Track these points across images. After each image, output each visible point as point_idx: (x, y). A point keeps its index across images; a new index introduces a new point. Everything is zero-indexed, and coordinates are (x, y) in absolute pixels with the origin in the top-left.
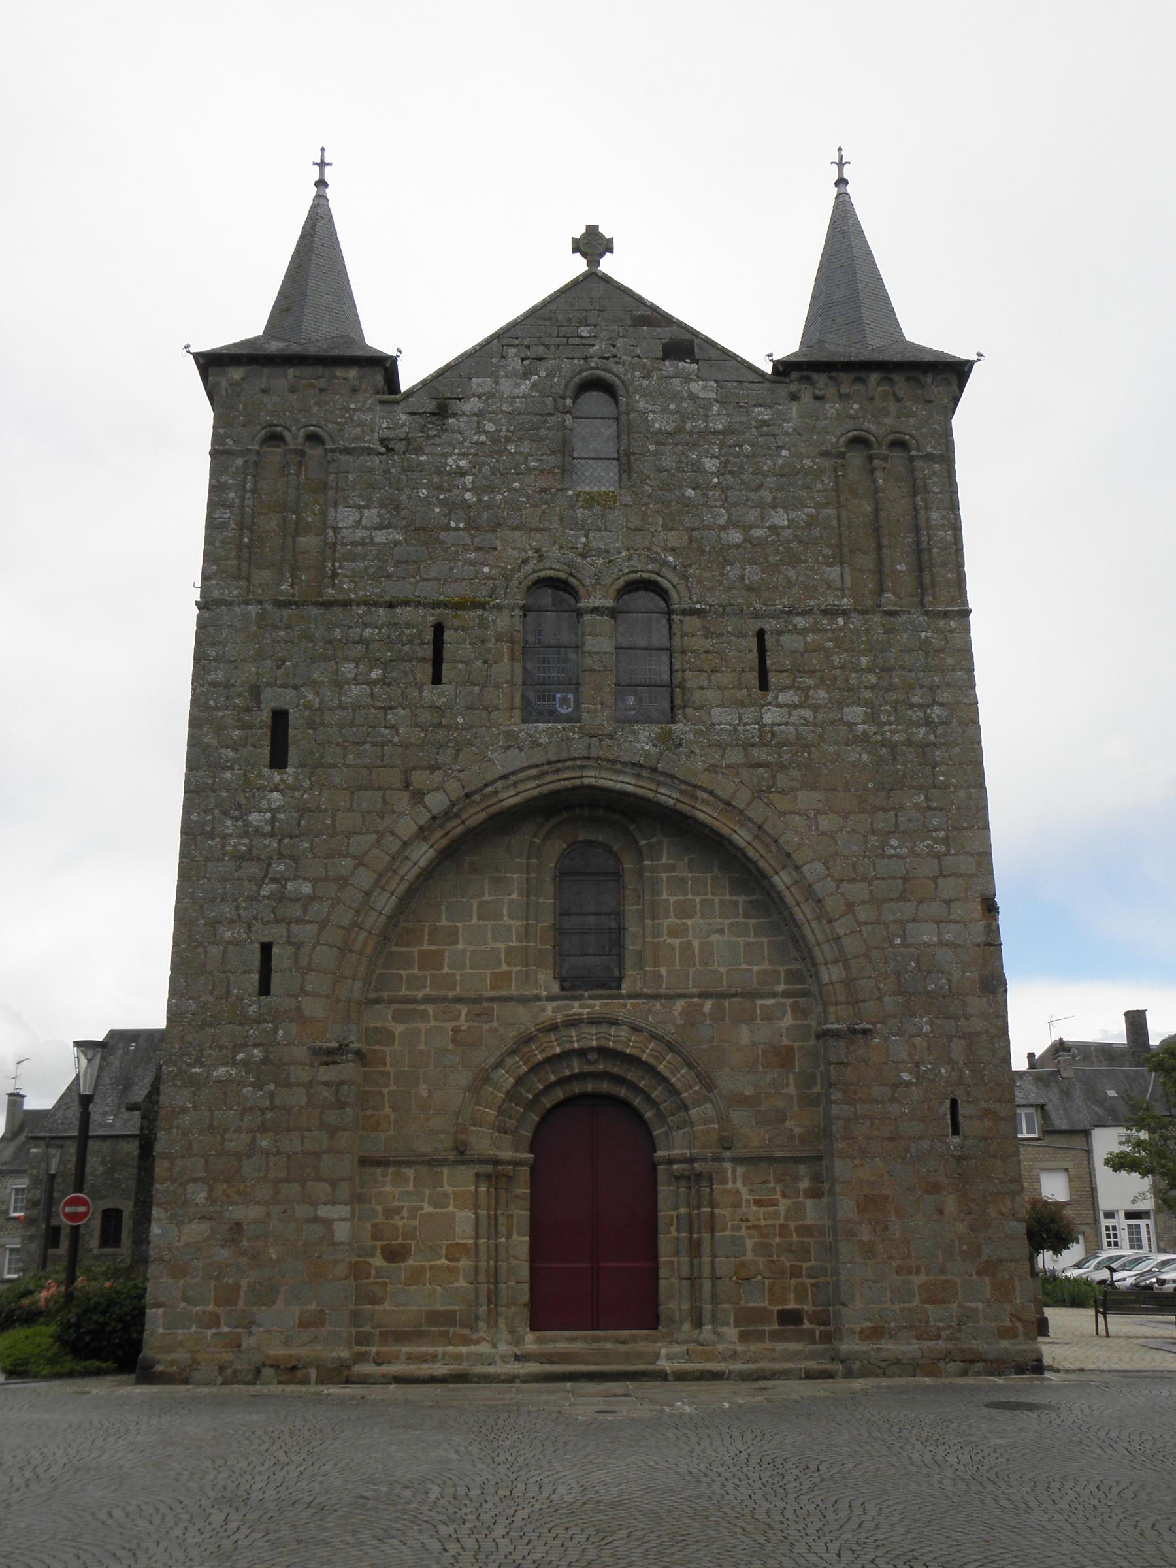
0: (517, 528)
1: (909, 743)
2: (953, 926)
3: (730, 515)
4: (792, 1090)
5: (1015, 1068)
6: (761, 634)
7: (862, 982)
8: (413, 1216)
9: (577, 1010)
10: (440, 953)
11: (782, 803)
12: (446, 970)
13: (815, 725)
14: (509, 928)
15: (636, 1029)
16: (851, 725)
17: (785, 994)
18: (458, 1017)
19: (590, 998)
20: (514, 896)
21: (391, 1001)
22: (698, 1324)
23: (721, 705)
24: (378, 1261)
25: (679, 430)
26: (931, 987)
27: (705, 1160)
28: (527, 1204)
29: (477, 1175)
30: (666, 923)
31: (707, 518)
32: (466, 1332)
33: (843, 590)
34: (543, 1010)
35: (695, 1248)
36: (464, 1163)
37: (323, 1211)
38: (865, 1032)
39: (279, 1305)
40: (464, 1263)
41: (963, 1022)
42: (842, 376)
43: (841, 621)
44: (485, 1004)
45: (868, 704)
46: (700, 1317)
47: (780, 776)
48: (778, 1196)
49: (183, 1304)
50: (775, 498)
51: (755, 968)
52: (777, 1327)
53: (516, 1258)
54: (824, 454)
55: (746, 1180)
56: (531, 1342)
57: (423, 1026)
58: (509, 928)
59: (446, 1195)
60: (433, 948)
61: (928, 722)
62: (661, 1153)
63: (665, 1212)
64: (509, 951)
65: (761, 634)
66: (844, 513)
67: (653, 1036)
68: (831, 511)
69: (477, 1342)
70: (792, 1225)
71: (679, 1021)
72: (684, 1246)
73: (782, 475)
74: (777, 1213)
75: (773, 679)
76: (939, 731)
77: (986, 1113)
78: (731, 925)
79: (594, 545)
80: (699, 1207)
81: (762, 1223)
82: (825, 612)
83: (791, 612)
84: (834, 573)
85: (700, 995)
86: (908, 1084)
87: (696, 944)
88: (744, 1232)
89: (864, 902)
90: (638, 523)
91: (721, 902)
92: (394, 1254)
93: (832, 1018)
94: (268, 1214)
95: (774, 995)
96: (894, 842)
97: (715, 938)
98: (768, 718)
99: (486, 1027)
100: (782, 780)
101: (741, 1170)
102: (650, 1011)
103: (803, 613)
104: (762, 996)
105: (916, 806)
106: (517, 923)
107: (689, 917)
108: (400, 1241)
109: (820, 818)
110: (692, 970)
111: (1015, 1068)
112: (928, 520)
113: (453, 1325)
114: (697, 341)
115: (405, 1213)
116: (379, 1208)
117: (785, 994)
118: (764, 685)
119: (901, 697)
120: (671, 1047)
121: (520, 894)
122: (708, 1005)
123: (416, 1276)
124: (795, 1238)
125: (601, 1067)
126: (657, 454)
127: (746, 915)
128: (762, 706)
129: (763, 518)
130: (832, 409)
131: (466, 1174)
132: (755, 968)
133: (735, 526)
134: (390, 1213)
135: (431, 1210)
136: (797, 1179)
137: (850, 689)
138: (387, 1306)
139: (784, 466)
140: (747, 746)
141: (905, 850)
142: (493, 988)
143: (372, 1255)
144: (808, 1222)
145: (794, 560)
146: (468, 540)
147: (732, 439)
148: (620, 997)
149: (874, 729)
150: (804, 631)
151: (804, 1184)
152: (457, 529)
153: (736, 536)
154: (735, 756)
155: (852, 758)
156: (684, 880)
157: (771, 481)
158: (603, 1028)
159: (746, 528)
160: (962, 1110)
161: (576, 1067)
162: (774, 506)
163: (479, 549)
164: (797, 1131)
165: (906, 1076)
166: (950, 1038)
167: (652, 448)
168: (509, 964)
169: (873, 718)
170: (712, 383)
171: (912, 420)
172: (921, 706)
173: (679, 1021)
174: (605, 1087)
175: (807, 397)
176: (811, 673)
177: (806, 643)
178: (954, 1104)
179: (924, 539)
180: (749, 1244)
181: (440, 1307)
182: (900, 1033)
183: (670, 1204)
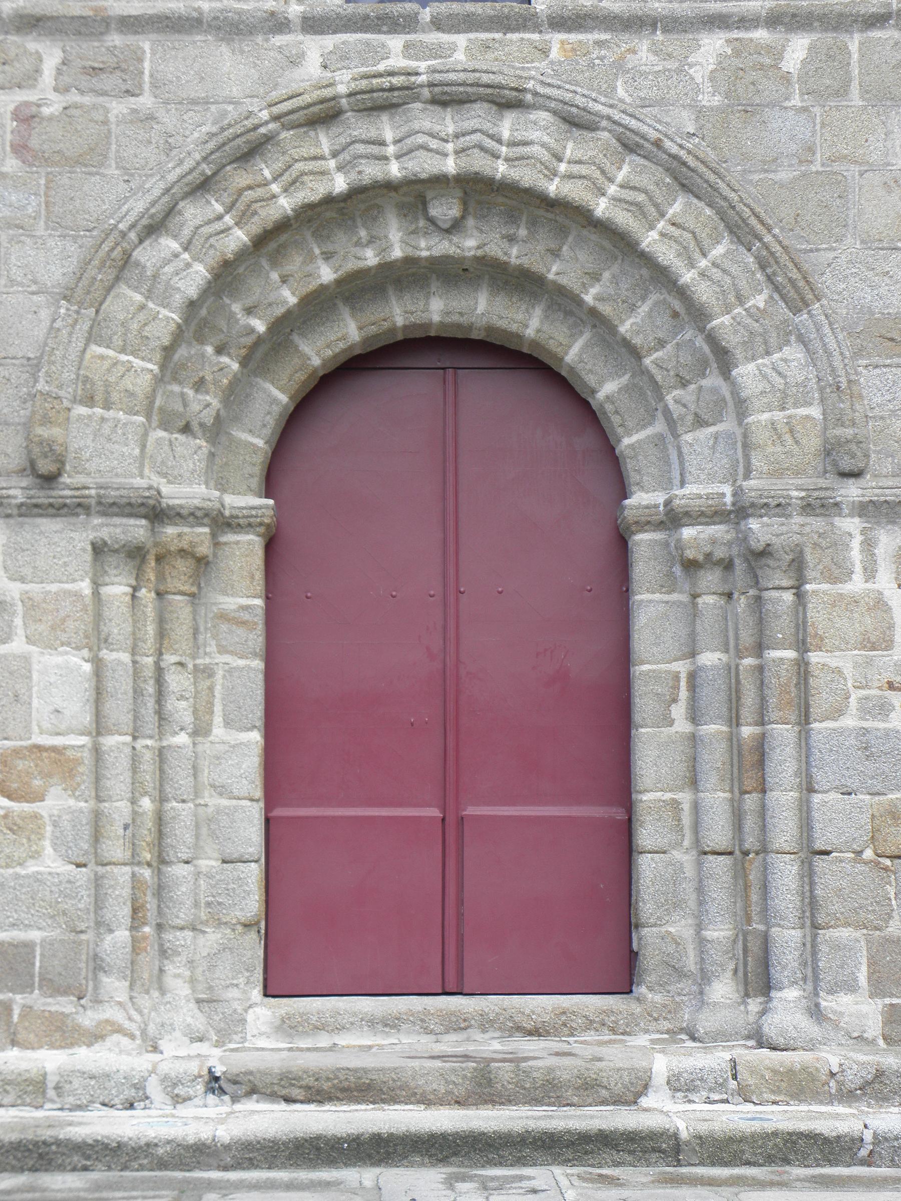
9: (397, 61)
15: (576, 121)
18: (31, 78)
19: (438, 24)
22: (759, 980)
27: (781, 508)
29: (99, 550)
32: (64, 1005)
35: (750, 766)
36: (59, 510)
40: (58, 803)
44: (116, 39)
46: (765, 963)
53: (221, 790)
56: (265, 1031)
62: (643, 499)
67: (630, 144)
69: (94, 1037)
71: (710, 99)
72: (715, 757)
80: (759, 648)
85: (774, 20)
99: (118, 108)
120: (683, 177)
122: (797, 49)
125: (469, 244)
158: (477, 117)
161: (396, 240)
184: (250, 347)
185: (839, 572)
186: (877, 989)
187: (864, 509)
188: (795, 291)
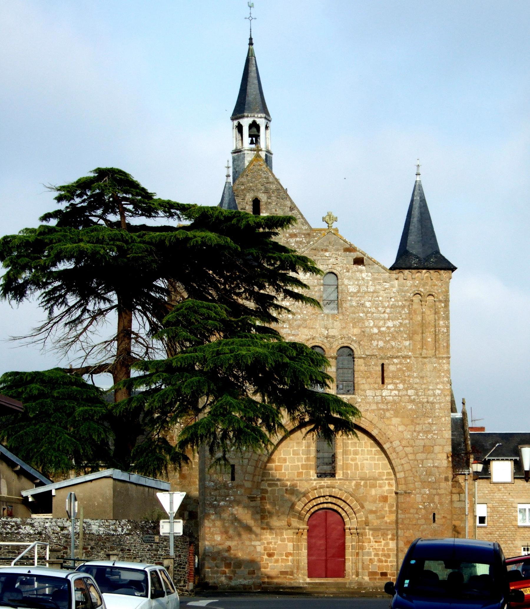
0: (305, 327)
1: (428, 402)
2: (438, 461)
3: (374, 323)
4: (387, 509)
5: (427, 562)
6: (383, 365)
7: (409, 478)
8: (275, 544)
10: (281, 466)
11: (387, 422)
12: (283, 471)
13: (399, 396)
14: (302, 458)
16: (409, 396)
17: (386, 479)
20: (304, 448)
21: (267, 480)
23: (370, 389)
24: (265, 557)
25: (359, 291)
26: (430, 480)
28: (306, 541)
29: (294, 533)
30: (350, 457)
31: (367, 324)
33: (410, 349)
34: (313, 483)
36: (290, 529)
37: (253, 543)
38: (409, 493)
39: (242, 568)
40: (290, 558)
41: (438, 491)
42: (413, 271)
43: (408, 361)
45: (416, 389)
47: (387, 413)
48: (382, 540)
49: (216, 568)
50: (389, 317)
51: (377, 471)
52: (380, 577)
54: (406, 300)
55: (372, 535)
57: (277, 488)
58: (302, 458)
59: (285, 539)
60: (279, 464)
61: (434, 395)
62: (347, 526)
63: (348, 544)
64: (302, 465)
65: (383, 365)
66: (411, 322)
68: (407, 321)
70: (386, 548)
71: (354, 488)
73: (392, 308)
74: (381, 545)
75: (386, 381)
76: (438, 398)
77: (444, 517)
78: (370, 458)
79: (330, 334)
81: (377, 547)
82: (403, 357)
83: (392, 357)
84: (407, 343)
86: (421, 509)
87: (359, 463)
88: (371, 550)
89: (411, 453)
90: (344, 326)
91: (367, 450)
92: (270, 555)
93: (400, 489)
94: (238, 544)
95: (383, 480)
96: (421, 435)
97: (365, 462)
98: (384, 394)
100: (388, 414)
101: (371, 532)
102: (345, 484)
103: (397, 357)
104: (379, 480)
105: (429, 423)
106: (305, 456)
107: (357, 455)
108: (272, 551)
109: (399, 426)
110: (358, 472)
111: (427, 562)
112: (439, 324)
113: (288, 575)
114: (365, 258)
115: (273, 543)
116: (265, 542)
117: (386, 479)
118: (383, 382)
119: (426, 387)
121: (305, 447)
122: (362, 483)
123: (277, 561)
124: (386, 552)
126: (351, 300)
127: (371, 447)
128: (382, 390)
129: (385, 323)
130: (409, 283)
131: (290, 532)
132: (377, 471)
133: (375, 327)
134: (269, 543)
135: (281, 543)
136: (387, 535)
137: (410, 384)
138: (268, 570)
139: (392, 305)
140: (377, 403)
141: (424, 437)
142: (297, 477)
143: (264, 555)
144: (390, 547)
145: (394, 338)
146: (290, 332)
147: (375, 295)
148: (336, 480)
149: (417, 397)
150: (397, 364)
151: (390, 537)
152: (286, 328)
153: (376, 331)
154: (374, 407)
155: (410, 407)
156: (356, 443)
157: (388, 310)
159: (379, 328)
160: (436, 516)
161: (322, 500)
162: (388, 319)
163: (293, 335)
164: (388, 521)
165: (421, 506)
166: (434, 495)
167: (349, 298)
168: (302, 469)
169: (417, 394)
170: (370, 274)
171: (436, 287)
172: (432, 390)
173: (354, 488)
174: (330, 506)
175: (401, 280)
176: (398, 379)
177: (397, 368)
178: (434, 514)
179: (437, 331)
180: (373, 553)
181: (283, 570)
182: (420, 493)
183: (350, 541)
184: (117, 338)
185: (366, 535)
186: (369, 576)
187: (369, 529)
188: (362, 507)
